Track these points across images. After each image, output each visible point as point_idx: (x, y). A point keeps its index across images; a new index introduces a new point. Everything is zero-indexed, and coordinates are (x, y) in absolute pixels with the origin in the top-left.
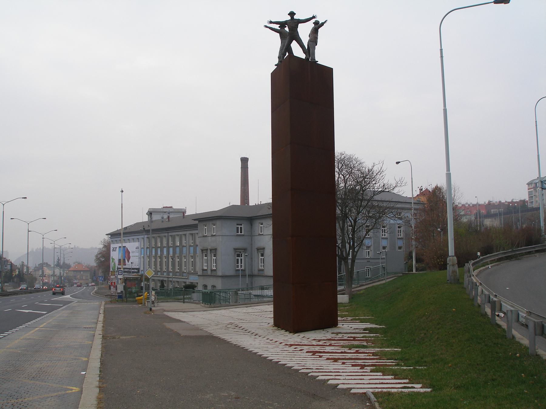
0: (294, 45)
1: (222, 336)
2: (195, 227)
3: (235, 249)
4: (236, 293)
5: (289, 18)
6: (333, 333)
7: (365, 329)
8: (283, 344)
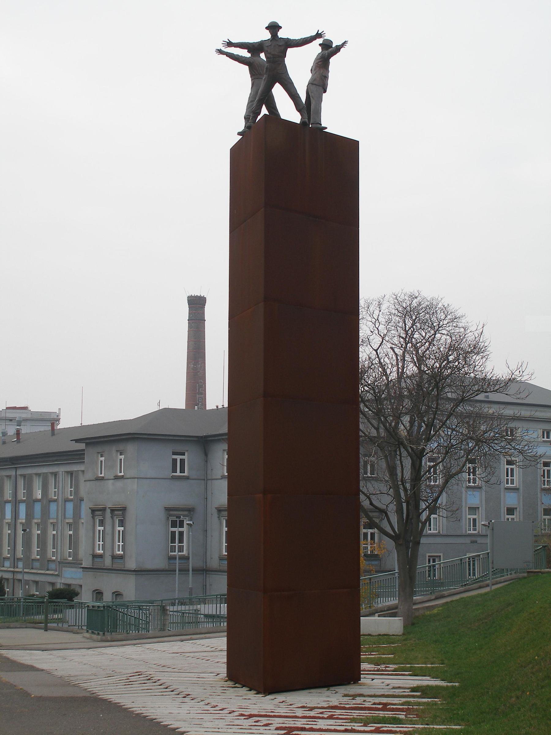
0: (278, 92)
1: (115, 699)
2: (75, 456)
3: (168, 510)
4: (164, 610)
5: (267, 35)
6: (346, 695)
7: (413, 689)
8: (236, 714)
